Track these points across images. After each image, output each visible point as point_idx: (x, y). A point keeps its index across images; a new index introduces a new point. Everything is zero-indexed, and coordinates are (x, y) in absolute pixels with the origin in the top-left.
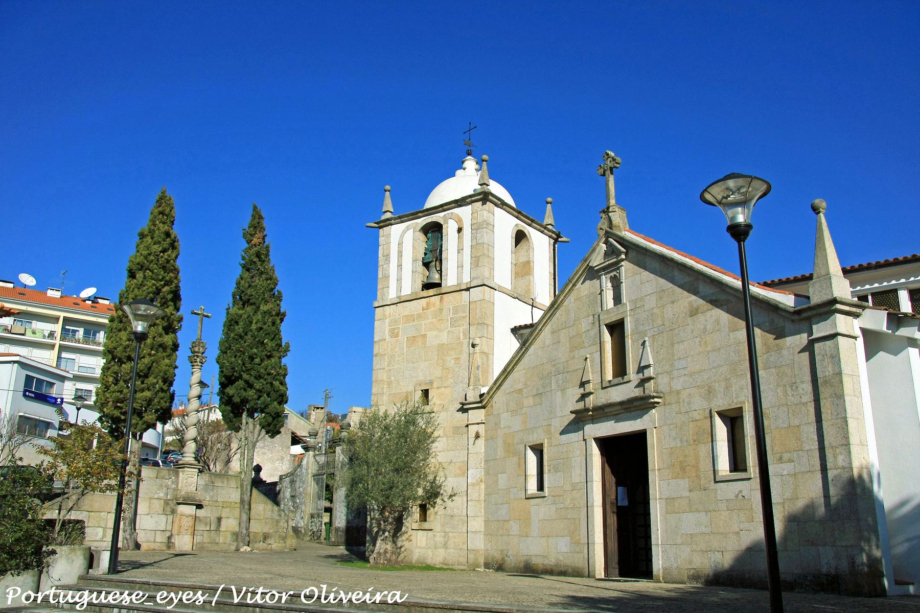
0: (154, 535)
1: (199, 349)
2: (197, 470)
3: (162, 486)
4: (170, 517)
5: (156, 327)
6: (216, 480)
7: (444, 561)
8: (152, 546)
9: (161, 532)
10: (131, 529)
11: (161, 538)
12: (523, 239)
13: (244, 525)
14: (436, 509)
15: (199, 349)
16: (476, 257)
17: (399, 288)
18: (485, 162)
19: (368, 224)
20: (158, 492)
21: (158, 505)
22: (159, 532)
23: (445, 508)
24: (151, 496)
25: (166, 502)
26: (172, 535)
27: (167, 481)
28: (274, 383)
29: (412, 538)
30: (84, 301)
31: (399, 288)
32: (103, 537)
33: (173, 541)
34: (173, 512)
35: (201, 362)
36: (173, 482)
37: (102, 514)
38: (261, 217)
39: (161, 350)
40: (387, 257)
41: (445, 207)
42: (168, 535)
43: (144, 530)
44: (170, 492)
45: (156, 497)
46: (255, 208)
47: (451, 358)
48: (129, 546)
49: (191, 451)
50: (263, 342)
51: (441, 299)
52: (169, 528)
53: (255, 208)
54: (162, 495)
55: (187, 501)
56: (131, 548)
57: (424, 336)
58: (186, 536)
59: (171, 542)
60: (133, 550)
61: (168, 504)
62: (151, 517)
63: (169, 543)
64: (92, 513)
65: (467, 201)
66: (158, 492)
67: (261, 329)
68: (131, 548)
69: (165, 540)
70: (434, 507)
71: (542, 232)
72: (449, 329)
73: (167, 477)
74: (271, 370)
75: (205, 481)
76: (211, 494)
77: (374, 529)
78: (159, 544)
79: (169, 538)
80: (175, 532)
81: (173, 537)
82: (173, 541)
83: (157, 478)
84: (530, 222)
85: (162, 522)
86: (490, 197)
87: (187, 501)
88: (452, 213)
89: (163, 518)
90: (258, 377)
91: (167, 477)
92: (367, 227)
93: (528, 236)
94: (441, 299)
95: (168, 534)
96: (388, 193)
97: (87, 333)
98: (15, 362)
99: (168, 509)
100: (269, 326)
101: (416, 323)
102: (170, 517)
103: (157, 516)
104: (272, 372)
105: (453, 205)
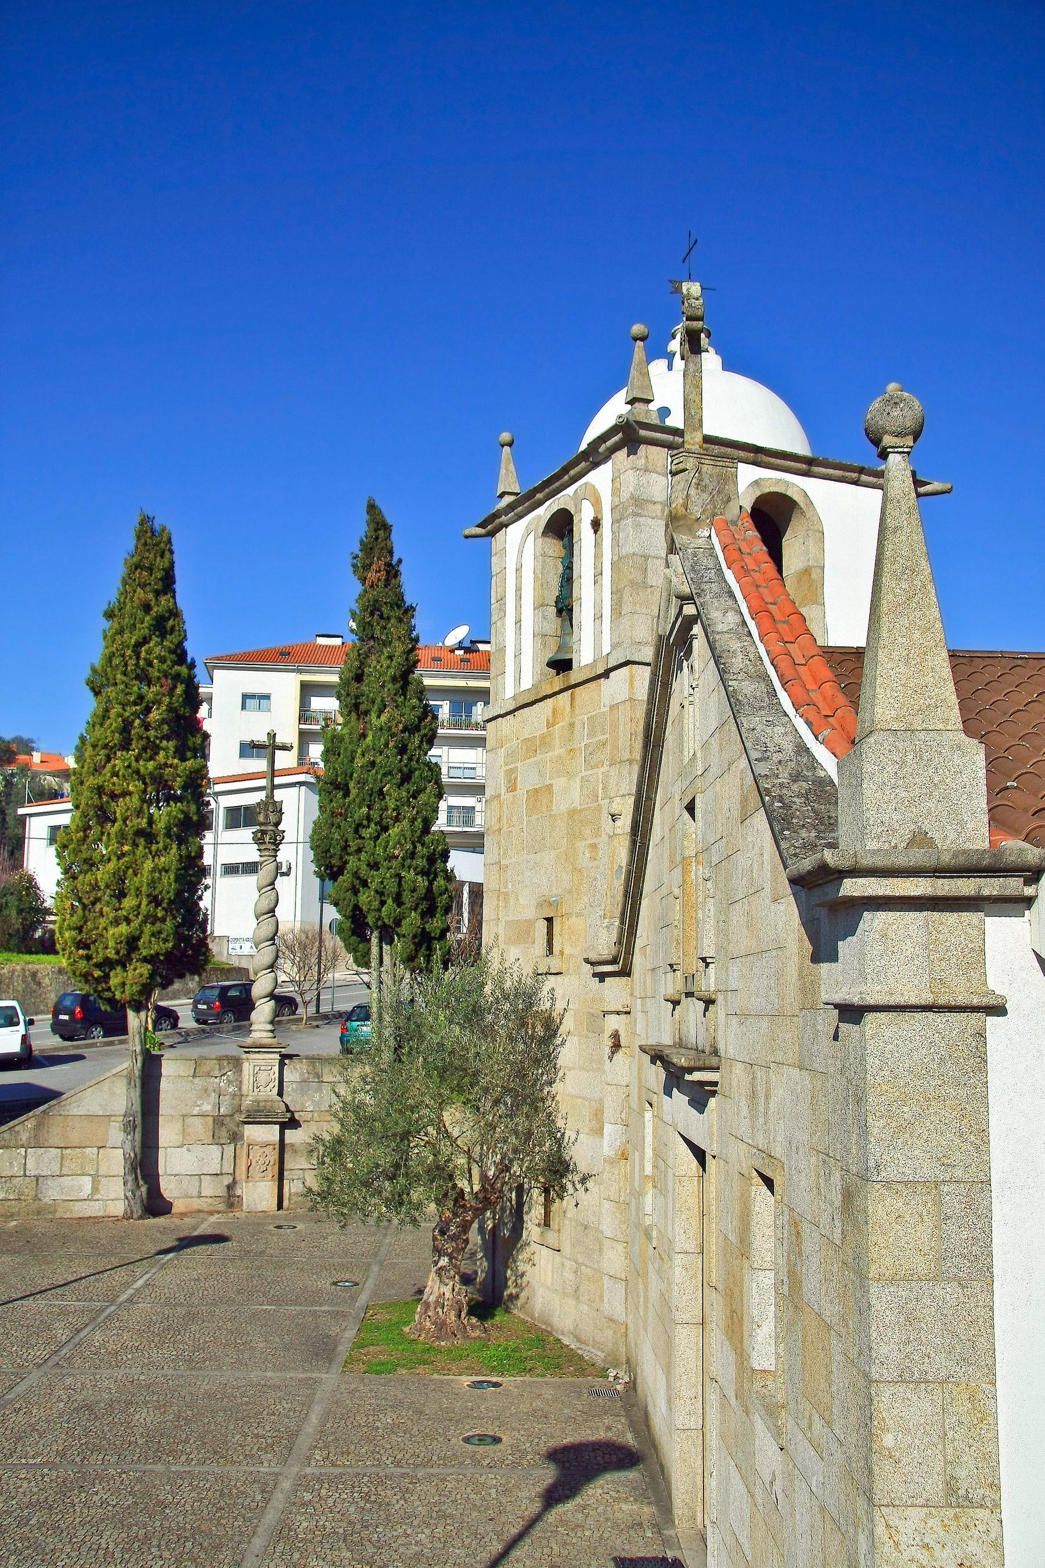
0: (198, 1184)
1: (267, 816)
2: (277, 1056)
3: (206, 1090)
4: (230, 1149)
5: (128, 798)
6: (326, 1070)
7: (575, 1328)
8: (196, 1204)
9: (213, 1178)
10: (136, 1178)
11: (212, 1189)
12: (793, 509)
13: (635, 1074)
14: (565, 1202)
15: (267, 816)
16: (618, 591)
17: (518, 680)
18: (639, 343)
19: (467, 532)
20: (199, 1103)
21: (200, 1128)
22: (208, 1177)
23: (577, 1205)
24: (184, 1113)
25: (219, 1121)
26: (235, 1182)
27: (217, 1080)
28: (403, 874)
29: (536, 1257)
30: (452, 651)
31: (518, 680)
32: (92, 1193)
33: (238, 1192)
34: (235, 1138)
35: (274, 844)
36: (230, 1082)
37: (88, 1150)
38: (387, 528)
39: (142, 841)
40: (502, 599)
41: (572, 473)
42: (226, 1183)
43: (176, 1175)
44: (226, 1101)
45: (195, 1112)
46: (372, 508)
47: (584, 843)
48: (132, 1212)
49: (263, 1020)
50: (381, 790)
51: (573, 698)
52: (228, 1168)
53: (372, 508)
54: (207, 1107)
55: (257, 1116)
56: (135, 1216)
57: (549, 787)
58: (262, 1184)
59: (234, 1196)
60: (141, 1218)
61: (223, 1124)
62: (189, 1150)
63: (231, 1199)
64: (68, 1151)
65: (601, 450)
66: (199, 1103)
67: (373, 764)
68: (135, 1216)
69: (222, 1192)
70: (562, 1198)
71: (856, 483)
72: (584, 774)
73: (217, 1073)
74: (395, 848)
75: (302, 1074)
76: (317, 1099)
77: (489, 1222)
78: (210, 1200)
79: (230, 1187)
80: (241, 1174)
81: (238, 1186)
82: (238, 1192)
83: (194, 1076)
84: (804, 466)
85: (212, 1158)
86: (643, 433)
87: (257, 1116)
88: (586, 484)
89: (215, 1151)
90: (374, 866)
91: (217, 1073)
92: (467, 537)
93: (802, 505)
94: (573, 698)
95: (227, 1180)
96: (507, 449)
97: (454, 710)
98: (301, 784)
99: (224, 1133)
100: (388, 757)
101: (539, 757)
102: (230, 1149)
103: (201, 1148)
104: (397, 852)
105: (583, 464)
